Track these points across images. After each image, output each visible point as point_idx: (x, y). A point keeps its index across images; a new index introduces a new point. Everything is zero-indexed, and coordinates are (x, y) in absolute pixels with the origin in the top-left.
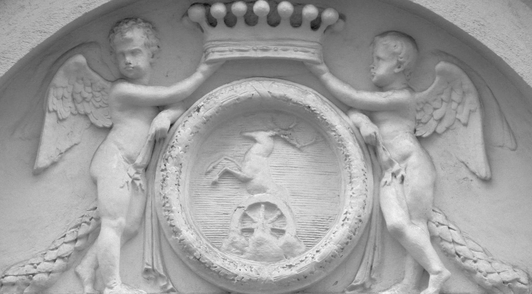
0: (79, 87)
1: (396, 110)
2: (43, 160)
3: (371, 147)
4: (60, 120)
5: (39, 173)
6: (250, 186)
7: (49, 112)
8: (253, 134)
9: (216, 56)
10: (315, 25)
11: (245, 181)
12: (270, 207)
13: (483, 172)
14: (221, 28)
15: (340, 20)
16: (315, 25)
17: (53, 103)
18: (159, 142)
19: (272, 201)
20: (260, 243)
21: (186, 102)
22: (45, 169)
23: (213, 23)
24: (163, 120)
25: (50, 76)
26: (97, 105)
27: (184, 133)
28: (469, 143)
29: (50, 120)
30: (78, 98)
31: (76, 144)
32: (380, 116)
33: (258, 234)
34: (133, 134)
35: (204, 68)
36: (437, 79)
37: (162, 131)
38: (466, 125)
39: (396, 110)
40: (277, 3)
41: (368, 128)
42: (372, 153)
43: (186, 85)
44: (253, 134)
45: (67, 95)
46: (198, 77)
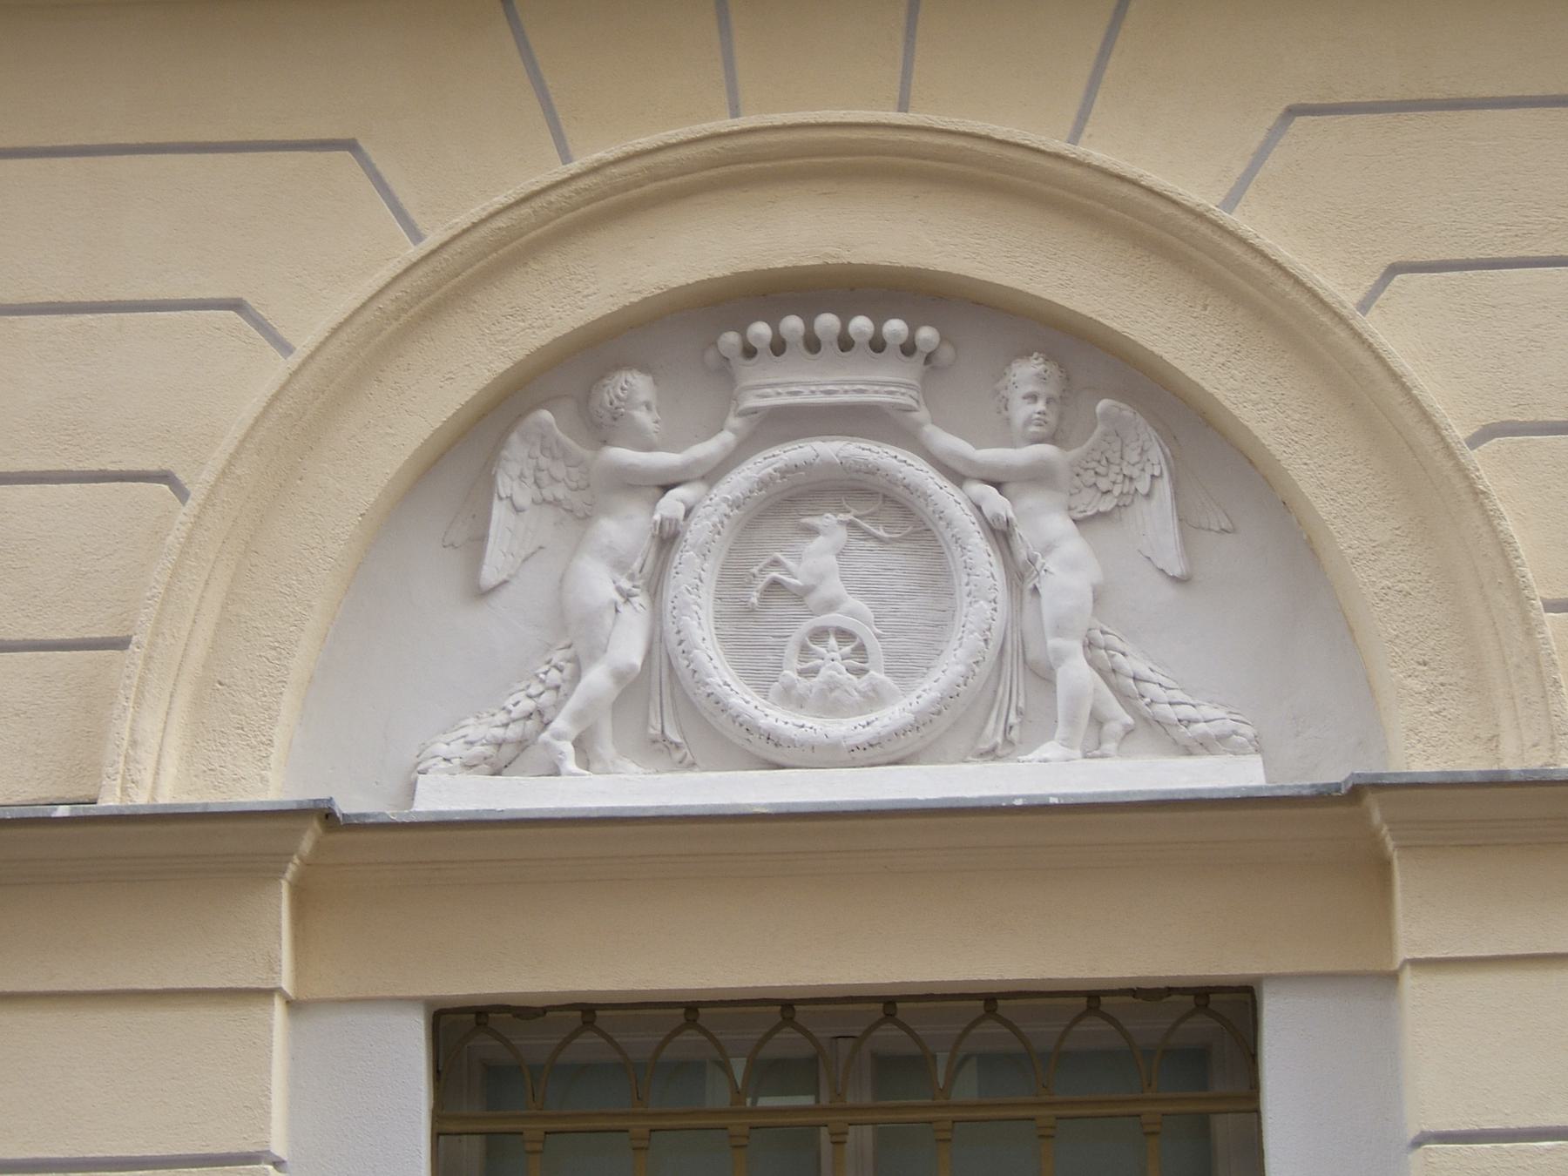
0: (544, 462)
1: (1038, 477)
2: (489, 576)
3: (1001, 534)
4: (518, 510)
5: (482, 594)
6: (812, 600)
7: (501, 498)
8: (815, 521)
9: (752, 402)
10: (908, 349)
11: (799, 595)
12: (844, 635)
13: (1177, 570)
14: (765, 355)
15: (563, 770)
16: (908, 349)
17: (506, 484)
18: (667, 539)
19: (845, 626)
20: (832, 686)
21: (712, 474)
22: (494, 589)
23: (749, 352)
24: (671, 505)
25: (501, 441)
26: (574, 485)
27: (697, 531)
28: (1155, 523)
29: (499, 511)
30: (544, 476)
31: (505, 582)
32: (1010, 489)
33: (825, 673)
34: (624, 528)
35: (734, 422)
36: (1100, 429)
37: (673, 521)
38: (1148, 496)
39: (1038, 477)
40: (849, 319)
41: (995, 503)
42: (1003, 544)
43: (708, 449)
44: (815, 521)
45: (528, 473)
46: (726, 438)
